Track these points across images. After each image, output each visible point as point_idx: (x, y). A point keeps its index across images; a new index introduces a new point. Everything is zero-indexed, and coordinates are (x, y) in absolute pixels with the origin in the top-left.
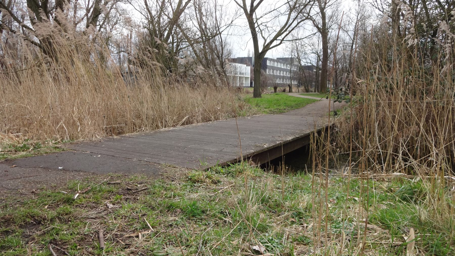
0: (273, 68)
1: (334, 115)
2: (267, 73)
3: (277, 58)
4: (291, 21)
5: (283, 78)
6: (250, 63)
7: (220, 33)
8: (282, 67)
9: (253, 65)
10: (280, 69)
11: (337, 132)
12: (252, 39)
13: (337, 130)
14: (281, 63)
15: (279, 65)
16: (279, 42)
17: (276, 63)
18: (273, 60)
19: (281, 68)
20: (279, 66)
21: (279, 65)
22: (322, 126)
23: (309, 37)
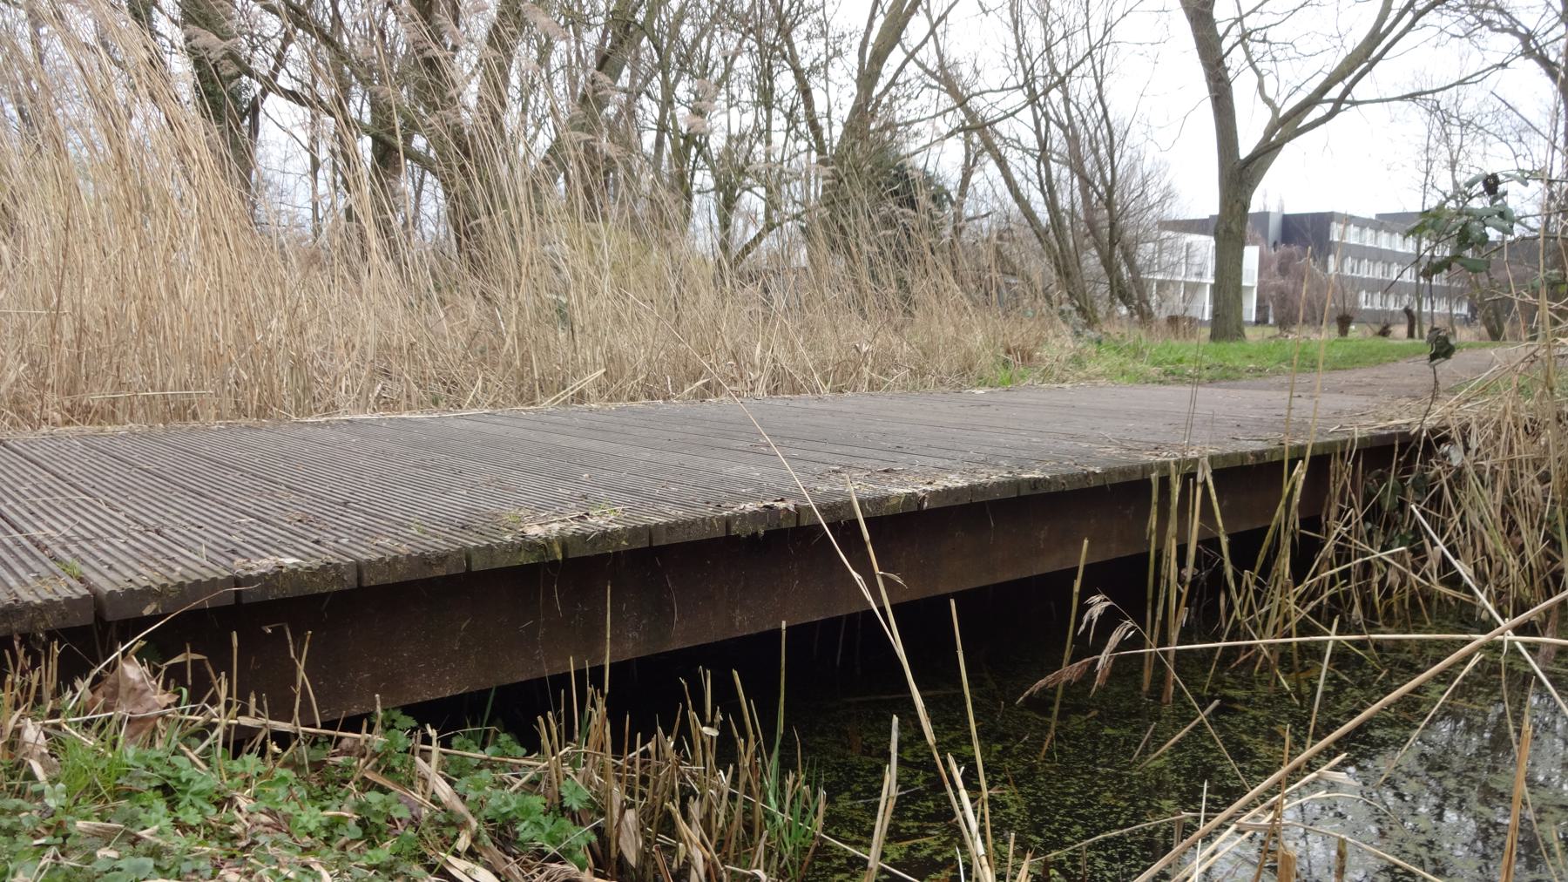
0: (1361, 253)
1: (1433, 357)
2: (1332, 267)
3: (1379, 216)
4: (1392, 16)
5: (1387, 288)
6: (1258, 235)
7: (1062, 81)
8: (1400, 250)
9: (1271, 243)
10: (1379, 256)
11: (1459, 477)
12: (1209, 102)
13: (1456, 463)
14: (1392, 232)
15: (1385, 241)
16: (1328, 107)
17: (1369, 233)
18: (1363, 224)
19: (1394, 253)
20: (1384, 246)
21: (1385, 241)
22: (1348, 433)
23: (1474, 79)
